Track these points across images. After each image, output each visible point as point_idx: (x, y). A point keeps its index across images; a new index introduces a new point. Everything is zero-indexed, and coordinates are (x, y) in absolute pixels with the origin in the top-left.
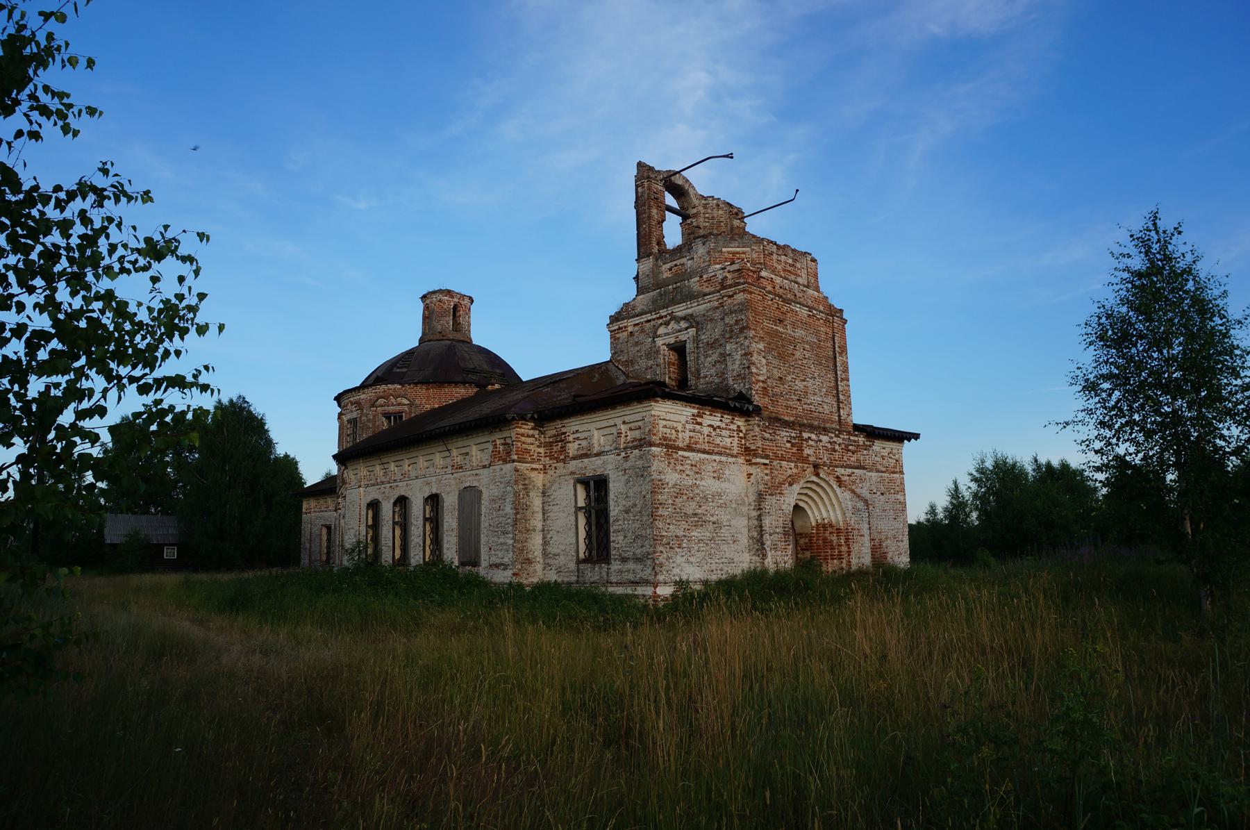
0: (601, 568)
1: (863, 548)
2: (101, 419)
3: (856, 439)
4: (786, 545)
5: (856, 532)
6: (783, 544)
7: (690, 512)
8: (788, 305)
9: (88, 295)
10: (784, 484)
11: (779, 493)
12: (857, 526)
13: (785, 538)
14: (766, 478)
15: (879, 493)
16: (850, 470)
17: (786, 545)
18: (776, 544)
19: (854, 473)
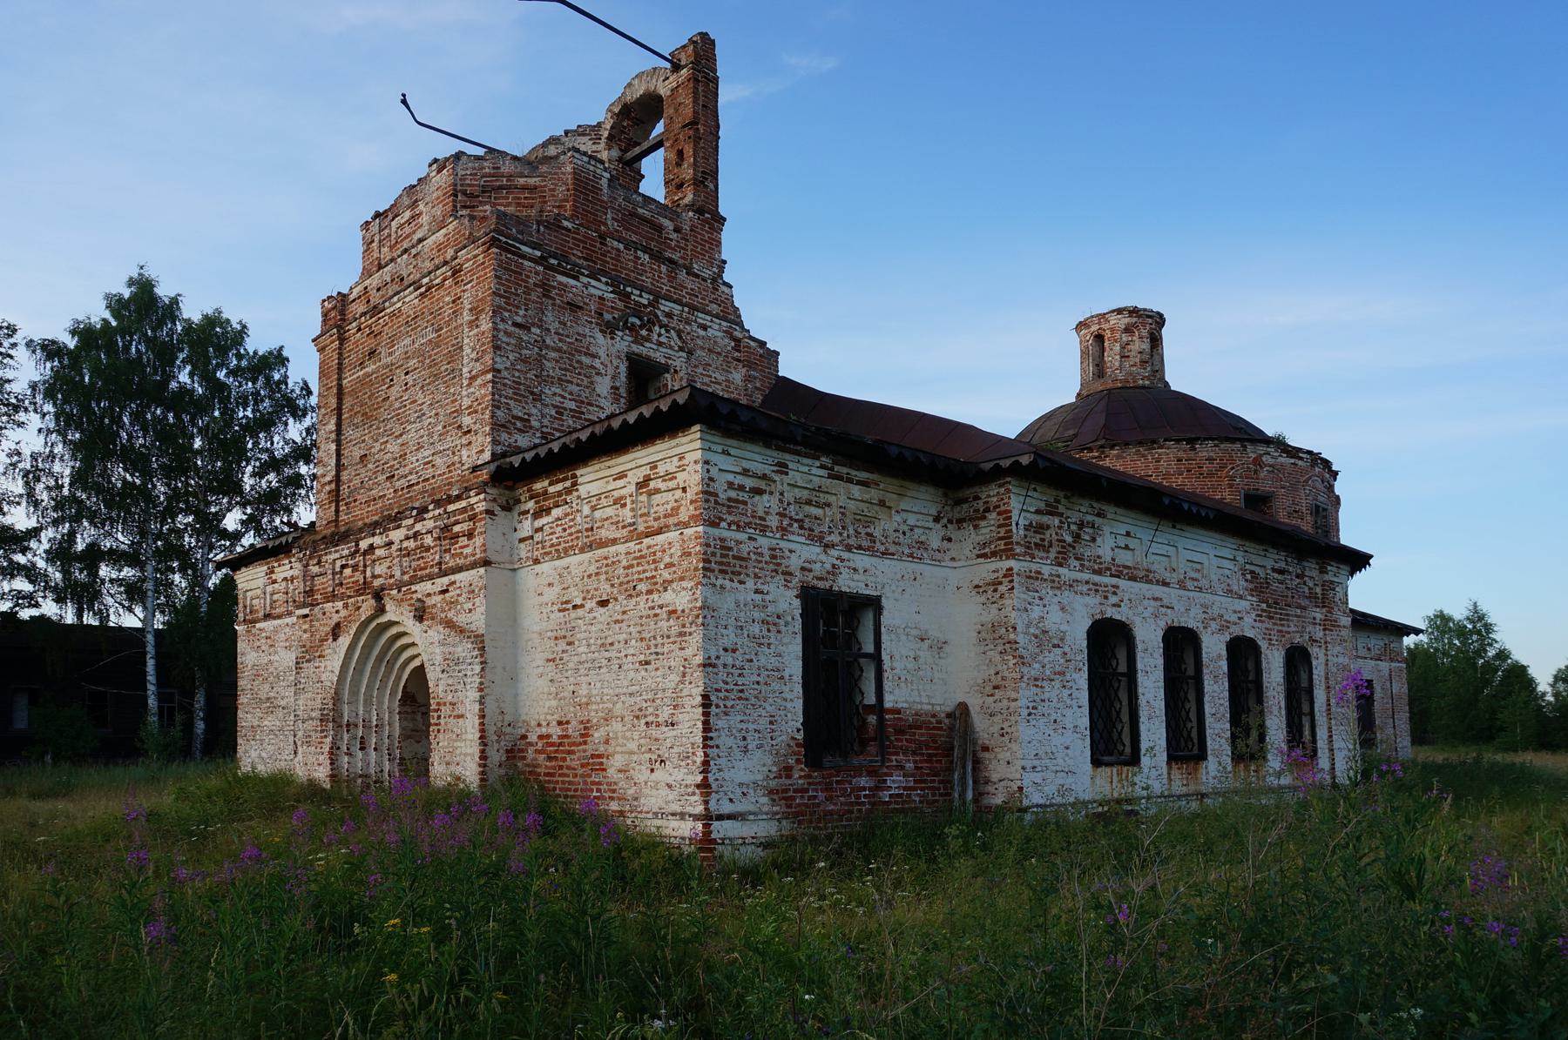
0: (1247, 769)
1: (459, 744)
2: (1371, 556)
3: (463, 504)
4: (322, 737)
5: (445, 710)
6: (319, 735)
7: (264, 697)
8: (383, 314)
9: (90, 619)
10: (327, 640)
11: (319, 657)
12: (450, 697)
13: (321, 726)
14: (305, 636)
15: (590, 604)
16: (446, 580)
17: (322, 737)
18: (310, 736)
19: (454, 583)
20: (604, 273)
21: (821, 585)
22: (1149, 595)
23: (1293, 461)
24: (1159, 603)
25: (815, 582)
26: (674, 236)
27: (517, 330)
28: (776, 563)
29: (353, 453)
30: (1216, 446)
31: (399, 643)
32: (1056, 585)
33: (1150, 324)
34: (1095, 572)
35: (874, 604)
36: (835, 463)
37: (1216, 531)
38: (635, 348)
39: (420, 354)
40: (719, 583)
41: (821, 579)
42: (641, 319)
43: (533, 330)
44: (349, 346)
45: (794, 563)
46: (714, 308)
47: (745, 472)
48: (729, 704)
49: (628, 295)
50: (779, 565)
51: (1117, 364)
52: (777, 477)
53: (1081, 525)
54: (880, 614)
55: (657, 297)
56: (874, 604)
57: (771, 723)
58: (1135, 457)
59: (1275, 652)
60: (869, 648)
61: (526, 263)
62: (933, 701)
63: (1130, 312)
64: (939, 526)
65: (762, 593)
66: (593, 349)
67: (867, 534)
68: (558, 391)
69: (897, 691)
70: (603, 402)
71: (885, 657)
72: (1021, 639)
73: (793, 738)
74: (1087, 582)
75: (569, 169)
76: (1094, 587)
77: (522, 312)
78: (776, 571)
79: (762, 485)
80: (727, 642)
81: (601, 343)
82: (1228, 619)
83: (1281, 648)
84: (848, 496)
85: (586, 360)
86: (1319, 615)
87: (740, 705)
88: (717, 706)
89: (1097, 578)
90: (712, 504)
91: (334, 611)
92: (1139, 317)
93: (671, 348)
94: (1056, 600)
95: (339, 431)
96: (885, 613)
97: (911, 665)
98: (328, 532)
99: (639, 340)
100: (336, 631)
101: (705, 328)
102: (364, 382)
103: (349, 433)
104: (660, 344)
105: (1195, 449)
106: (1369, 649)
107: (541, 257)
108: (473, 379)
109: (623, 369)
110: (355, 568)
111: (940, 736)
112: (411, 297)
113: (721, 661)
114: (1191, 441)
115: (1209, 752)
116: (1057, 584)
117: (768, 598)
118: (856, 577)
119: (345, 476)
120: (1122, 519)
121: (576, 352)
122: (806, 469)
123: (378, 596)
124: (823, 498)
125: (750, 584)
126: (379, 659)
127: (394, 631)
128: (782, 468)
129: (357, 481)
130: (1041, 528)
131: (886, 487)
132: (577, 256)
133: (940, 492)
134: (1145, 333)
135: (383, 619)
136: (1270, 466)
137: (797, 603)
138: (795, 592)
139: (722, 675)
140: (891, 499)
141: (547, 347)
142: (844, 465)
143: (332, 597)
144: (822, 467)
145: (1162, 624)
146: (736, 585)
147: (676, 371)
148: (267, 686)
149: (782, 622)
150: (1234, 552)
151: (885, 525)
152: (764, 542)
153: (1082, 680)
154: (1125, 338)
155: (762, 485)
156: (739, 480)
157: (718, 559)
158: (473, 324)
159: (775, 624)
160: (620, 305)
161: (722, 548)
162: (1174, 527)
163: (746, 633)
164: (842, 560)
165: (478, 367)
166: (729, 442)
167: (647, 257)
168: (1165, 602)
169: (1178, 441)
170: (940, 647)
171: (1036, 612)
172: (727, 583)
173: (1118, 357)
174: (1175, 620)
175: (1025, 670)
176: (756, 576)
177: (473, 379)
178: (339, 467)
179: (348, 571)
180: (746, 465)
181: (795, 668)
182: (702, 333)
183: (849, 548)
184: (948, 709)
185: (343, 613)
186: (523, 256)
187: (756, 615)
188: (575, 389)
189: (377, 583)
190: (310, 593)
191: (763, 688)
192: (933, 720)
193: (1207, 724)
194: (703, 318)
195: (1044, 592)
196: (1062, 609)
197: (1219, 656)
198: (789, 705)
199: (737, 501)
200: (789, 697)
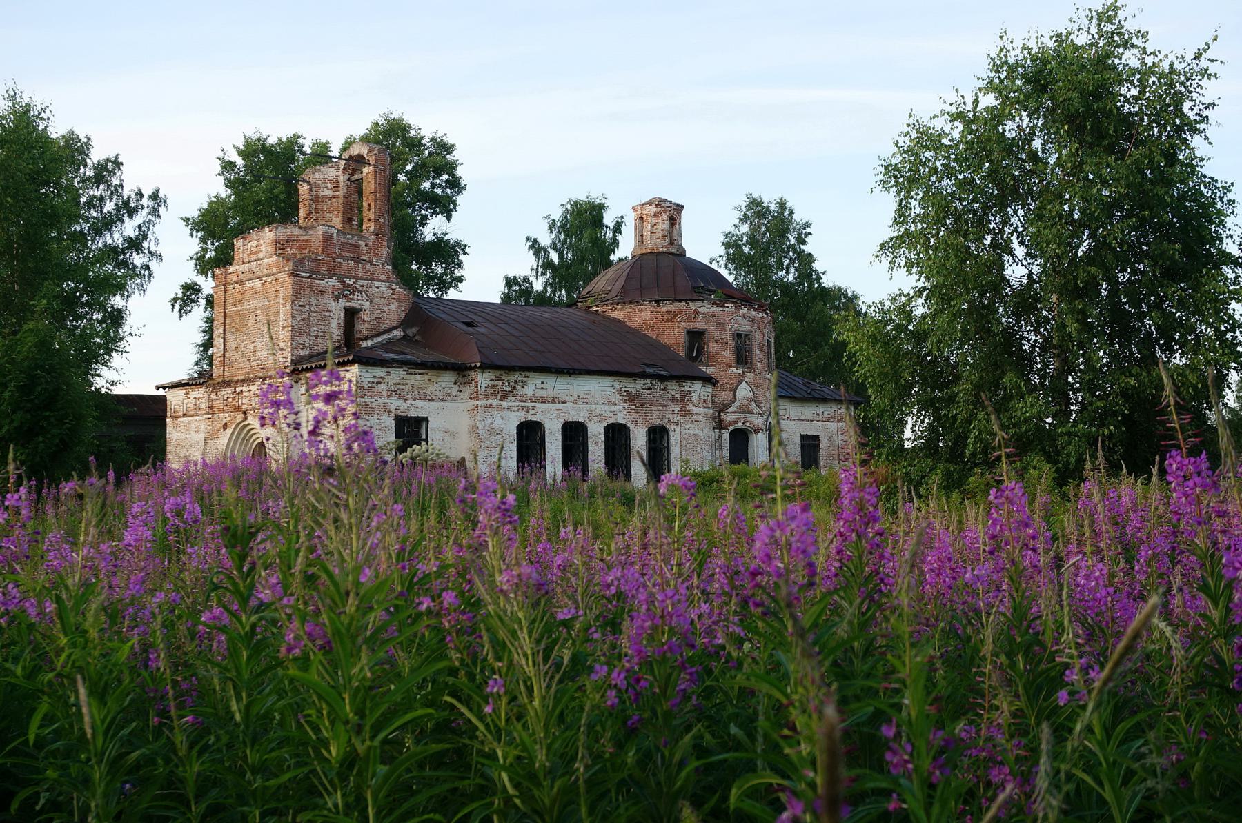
20: (335, 275)
26: (365, 248)
29: (231, 345)
31: (252, 432)
35: (426, 420)
38: (348, 304)
39: (261, 308)
44: (229, 294)
45: (392, 408)
46: (383, 277)
53: (516, 382)
55: (357, 279)
56: (426, 420)
59: (640, 430)
60: (424, 437)
72: (480, 432)
84: (416, 379)
85: (327, 314)
86: (677, 409)
89: (523, 404)
91: (224, 417)
95: (224, 334)
98: (220, 380)
99: (349, 300)
100: (225, 427)
101: (378, 288)
102: (236, 313)
103: (229, 335)
108: (284, 327)
109: (342, 314)
110: (234, 399)
112: (257, 283)
114: (657, 302)
116: (500, 408)
119: (227, 355)
121: (323, 312)
123: (245, 413)
125: (375, 417)
126: (243, 439)
127: (250, 427)
128: (388, 373)
129: (233, 358)
130: (493, 387)
131: (431, 375)
134: (665, 217)
135: (246, 422)
140: (433, 378)
143: (223, 411)
145: (563, 421)
148: (184, 450)
151: (431, 388)
152: (381, 401)
154: (654, 221)
158: (284, 305)
160: (341, 287)
165: (286, 324)
169: (650, 302)
170: (454, 435)
171: (489, 421)
177: (284, 327)
178: (225, 350)
179: (230, 400)
183: (415, 400)
185: (229, 419)
188: (322, 327)
189: (244, 407)
190: (211, 408)
194: (377, 284)
197: (599, 434)
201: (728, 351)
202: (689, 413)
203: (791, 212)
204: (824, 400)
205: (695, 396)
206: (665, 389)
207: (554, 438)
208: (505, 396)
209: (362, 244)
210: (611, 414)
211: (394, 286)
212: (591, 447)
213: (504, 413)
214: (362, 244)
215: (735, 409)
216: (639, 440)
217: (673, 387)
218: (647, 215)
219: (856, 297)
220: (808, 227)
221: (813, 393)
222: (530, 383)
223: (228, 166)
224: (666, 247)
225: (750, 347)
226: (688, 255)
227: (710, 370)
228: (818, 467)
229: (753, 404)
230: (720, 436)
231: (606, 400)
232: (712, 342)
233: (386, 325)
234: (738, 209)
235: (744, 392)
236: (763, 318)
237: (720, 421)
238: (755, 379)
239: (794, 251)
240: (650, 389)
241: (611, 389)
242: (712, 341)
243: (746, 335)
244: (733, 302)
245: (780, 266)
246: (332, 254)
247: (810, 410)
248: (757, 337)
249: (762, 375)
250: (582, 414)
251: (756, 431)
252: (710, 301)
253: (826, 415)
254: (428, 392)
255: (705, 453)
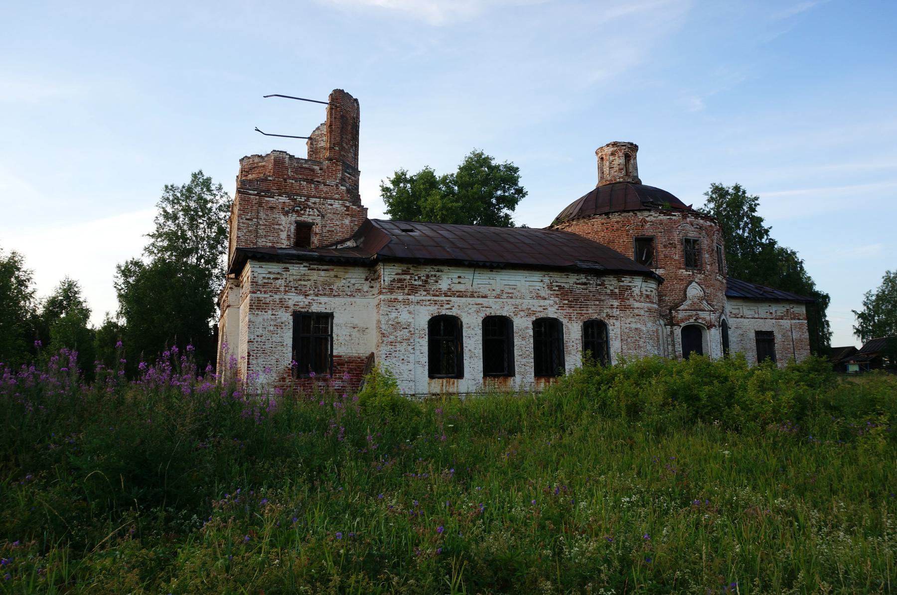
21: (303, 310)
22: (473, 302)
23: (668, 217)
24: (480, 306)
25: (300, 309)
26: (320, 172)
27: (247, 221)
28: (282, 304)
30: (619, 215)
32: (407, 303)
33: (630, 151)
34: (434, 295)
36: (310, 264)
37: (524, 270)
38: (298, 219)
40: (256, 312)
41: (301, 308)
42: (300, 207)
43: (254, 220)
46: (337, 196)
47: (270, 273)
48: (258, 355)
49: (296, 199)
50: (283, 304)
51: (608, 172)
52: (284, 273)
53: (428, 276)
54: (333, 319)
55: (308, 197)
57: (277, 362)
58: (584, 224)
59: (575, 324)
61: (252, 196)
62: (359, 352)
63: (613, 145)
64: (368, 282)
65: (275, 315)
66: (280, 222)
67: (330, 289)
68: (264, 240)
69: (339, 349)
70: (283, 241)
71: (334, 336)
73: (287, 367)
74: (429, 300)
75: (273, 158)
76: (434, 302)
77: (249, 215)
78: (282, 307)
79: (278, 276)
80: (259, 334)
81: (283, 220)
82: (535, 310)
83: (579, 322)
84: (319, 275)
85: (276, 227)
86: (616, 303)
87: (263, 355)
88: (253, 356)
90: (255, 286)
92: (618, 146)
93: (314, 216)
94: (406, 309)
96: (335, 319)
97: (348, 338)
99: (299, 215)
101: (331, 205)
104: (309, 215)
105: (609, 218)
106: (771, 313)
107: (258, 193)
109: (293, 228)
111: (362, 366)
113: (256, 340)
114: (607, 214)
115: (516, 373)
116: (406, 303)
117: (277, 317)
118: (320, 306)
120: (453, 271)
121: (272, 226)
122: (297, 268)
124: (306, 278)
125: (270, 312)
130: (400, 281)
132: (274, 189)
133: (366, 269)
134: (621, 154)
136: (651, 222)
137: (291, 318)
138: (290, 314)
139: (256, 345)
140: (341, 274)
141: (260, 225)
142: (315, 264)
144: (304, 267)
145: (483, 315)
146: (263, 313)
147: (317, 224)
149: (283, 325)
150: (541, 278)
151: (338, 284)
152: (277, 297)
153: (425, 342)
154: (612, 158)
155: (278, 276)
156: (268, 276)
157: (256, 304)
159: (280, 326)
160: (292, 203)
161: (258, 300)
162: (492, 271)
163: (267, 330)
164: (314, 300)
166: (262, 263)
167: (305, 183)
168: (485, 305)
169: (600, 215)
170: (364, 330)
171: (393, 315)
172: (260, 313)
173: (608, 168)
174: (493, 313)
175: (385, 339)
176: (273, 309)
180: (270, 270)
181: (289, 341)
182: (330, 207)
183: (317, 295)
184: (367, 355)
186: (251, 194)
187: (272, 323)
188: (271, 238)
191: (274, 349)
192: (359, 360)
193: (515, 360)
194: (329, 201)
195: (399, 306)
196: (410, 313)
197: (527, 328)
198: (285, 355)
199: (268, 283)
200: (286, 352)
201: (677, 255)
202: (629, 307)
203: (744, 192)
204: (777, 301)
205: (636, 291)
206: (602, 284)
207: (473, 332)
208: (414, 290)
209: (317, 168)
210: (540, 309)
211: (348, 204)
212: (517, 341)
213: (412, 308)
214: (317, 168)
215: (686, 307)
216: (573, 333)
217: (611, 283)
218: (606, 155)
219: (794, 253)
220: (757, 200)
221: (765, 294)
222: (444, 277)
223: (385, 190)
224: (622, 177)
225: (700, 251)
226: (643, 183)
227: (660, 272)
228: (773, 359)
229: (704, 302)
230: (672, 332)
231: (534, 295)
232: (660, 247)
233: (339, 237)
234: (707, 194)
235: (694, 291)
236: (711, 226)
237: (672, 318)
238: (705, 280)
239: (748, 217)
240: (585, 284)
241: (541, 284)
242: (660, 246)
243: (695, 241)
244: (680, 212)
245: (738, 227)
246: (283, 175)
247: (763, 310)
248: (705, 243)
249: (713, 276)
250: (506, 308)
251: (709, 327)
252: (657, 210)
253: (779, 314)
254: (335, 288)
255: (649, 347)
